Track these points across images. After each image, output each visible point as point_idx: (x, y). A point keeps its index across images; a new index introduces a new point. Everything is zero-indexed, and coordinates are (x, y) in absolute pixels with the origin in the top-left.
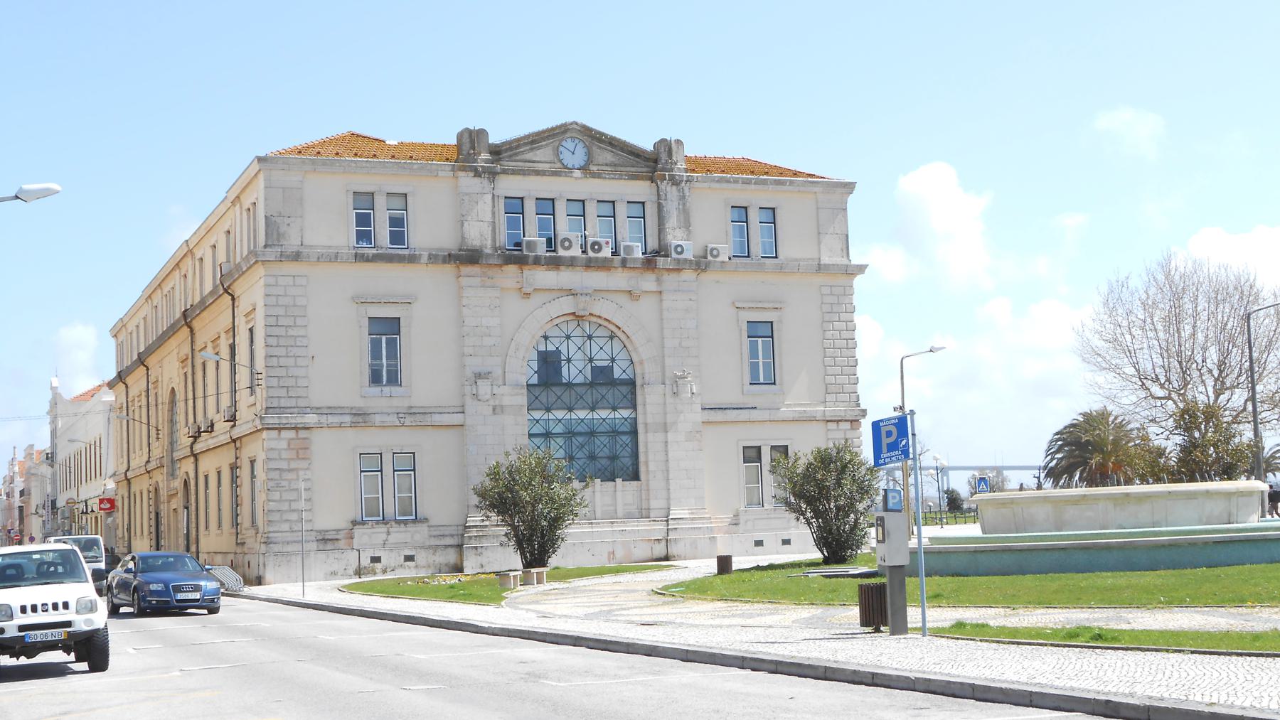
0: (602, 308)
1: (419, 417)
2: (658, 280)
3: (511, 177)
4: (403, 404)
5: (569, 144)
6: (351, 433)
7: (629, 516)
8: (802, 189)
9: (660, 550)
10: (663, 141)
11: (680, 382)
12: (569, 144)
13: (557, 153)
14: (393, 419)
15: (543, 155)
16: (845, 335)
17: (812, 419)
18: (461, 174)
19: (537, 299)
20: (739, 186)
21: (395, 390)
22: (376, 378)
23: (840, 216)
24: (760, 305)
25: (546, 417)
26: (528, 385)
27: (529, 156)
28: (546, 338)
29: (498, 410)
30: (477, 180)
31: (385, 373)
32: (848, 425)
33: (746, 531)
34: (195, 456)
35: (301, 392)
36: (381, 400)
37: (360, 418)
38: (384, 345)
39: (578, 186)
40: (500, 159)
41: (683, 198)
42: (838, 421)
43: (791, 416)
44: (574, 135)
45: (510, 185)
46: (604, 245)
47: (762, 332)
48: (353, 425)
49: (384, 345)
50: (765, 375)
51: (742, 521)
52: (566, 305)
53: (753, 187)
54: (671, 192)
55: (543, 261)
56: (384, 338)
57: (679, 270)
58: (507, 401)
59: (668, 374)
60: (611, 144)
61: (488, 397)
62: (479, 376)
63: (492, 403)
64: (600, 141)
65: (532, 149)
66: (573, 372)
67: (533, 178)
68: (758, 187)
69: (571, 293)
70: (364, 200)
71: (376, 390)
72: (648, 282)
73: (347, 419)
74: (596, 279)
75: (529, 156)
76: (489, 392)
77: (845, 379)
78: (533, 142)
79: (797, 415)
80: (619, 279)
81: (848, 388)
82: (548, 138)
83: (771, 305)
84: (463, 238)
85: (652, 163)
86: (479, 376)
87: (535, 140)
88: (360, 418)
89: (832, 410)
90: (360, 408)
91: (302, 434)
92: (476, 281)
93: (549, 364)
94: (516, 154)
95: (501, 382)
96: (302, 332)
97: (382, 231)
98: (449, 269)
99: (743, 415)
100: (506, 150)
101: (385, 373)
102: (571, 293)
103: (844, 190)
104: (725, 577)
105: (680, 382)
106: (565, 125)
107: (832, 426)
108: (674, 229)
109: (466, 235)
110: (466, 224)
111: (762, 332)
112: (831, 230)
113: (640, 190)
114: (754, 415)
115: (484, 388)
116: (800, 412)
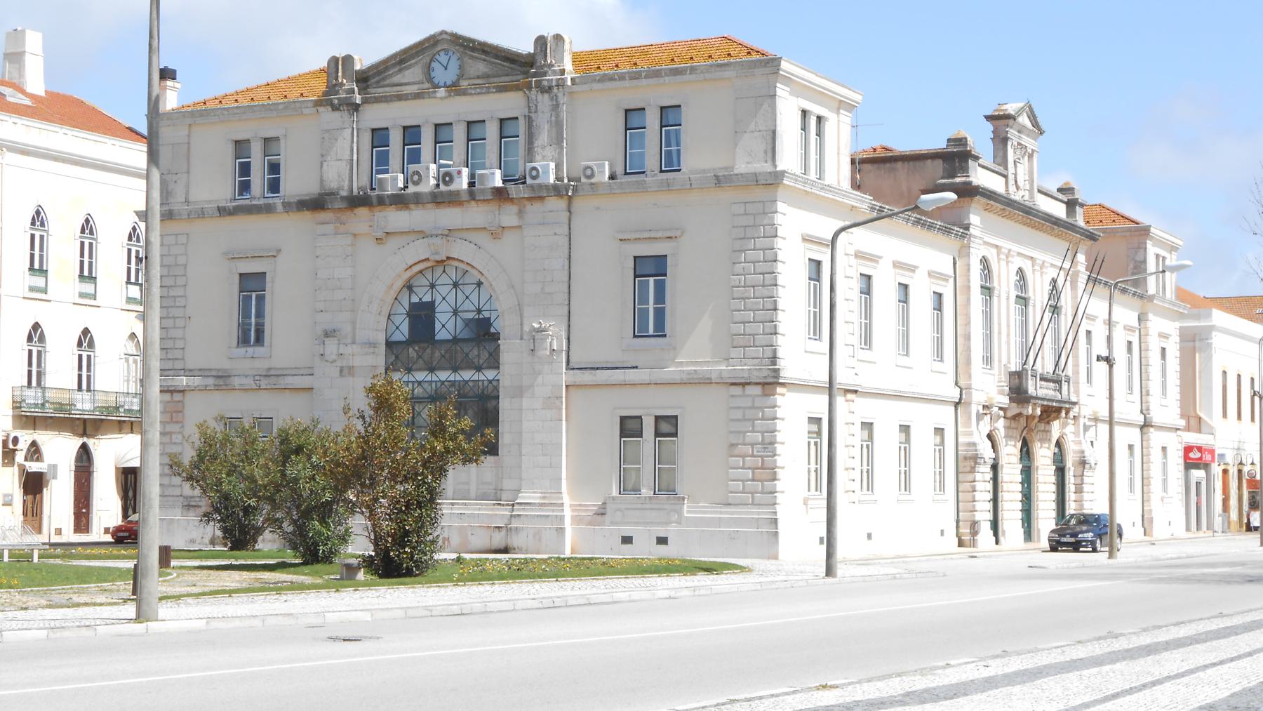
0: (460, 250)
1: (273, 379)
2: (521, 213)
3: (376, 106)
4: (262, 365)
5: (443, 58)
6: (217, 395)
7: (483, 497)
8: (708, 76)
9: (498, 540)
10: (334, 61)
11: (538, 336)
12: (443, 58)
13: (428, 70)
14: (249, 382)
15: (413, 74)
16: (761, 267)
17: (706, 382)
18: (321, 109)
19: (393, 243)
20: (627, 83)
21: (259, 350)
22: (244, 340)
23: (766, 106)
24: (646, 235)
25: (428, 378)
26: (390, 345)
27: (396, 79)
28: (479, 284)
29: (346, 371)
30: (337, 114)
31: (252, 333)
32: (757, 390)
33: (613, 523)
34: (831, 389)
35: (178, 354)
36: (247, 361)
37: (222, 381)
38: (254, 303)
39: (457, 109)
40: (368, 87)
41: (556, 107)
42: (744, 385)
43: (677, 378)
44: (445, 46)
45: (376, 115)
46: (455, 175)
47: (651, 269)
48: (218, 388)
49: (254, 303)
50: (651, 323)
51: (609, 511)
52: (419, 250)
53: (644, 82)
54: (544, 101)
55: (387, 201)
56: (254, 295)
57: (541, 198)
58: (357, 362)
59: (526, 328)
60: (484, 52)
61: (334, 357)
62: (328, 334)
63: (339, 363)
64: (473, 49)
65: (400, 70)
66: (445, 326)
67: (397, 104)
68: (650, 81)
69: (422, 234)
70: (241, 147)
71: (242, 351)
72: (508, 216)
73: (211, 381)
74: (449, 217)
75: (396, 79)
76: (335, 352)
77: (760, 328)
78: (401, 62)
79: (685, 377)
80: (475, 215)
81: (761, 339)
82: (417, 54)
83: (633, 236)
84: (322, 181)
85: (521, 69)
86: (328, 334)
87: (402, 59)
88: (222, 381)
89: (744, 369)
90: (225, 370)
91: (177, 397)
92: (329, 228)
93: (422, 316)
94: (384, 79)
95: (349, 341)
96: (180, 292)
97: (258, 179)
98: (307, 215)
99: (618, 376)
100: (374, 75)
101: (252, 333)
102: (422, 234)
103: (767, 70)
104: (830, 580)
105: (538, 336)
106: (432, 37)
107: (737, 390)
108: (544, 147)
109: (325, 178)
110: (325, 164)
111: (651, 269)
112: (752, 127)
113: (511, 103)
114: (631, 375)
115: (331, 347)
116: (689, 373)
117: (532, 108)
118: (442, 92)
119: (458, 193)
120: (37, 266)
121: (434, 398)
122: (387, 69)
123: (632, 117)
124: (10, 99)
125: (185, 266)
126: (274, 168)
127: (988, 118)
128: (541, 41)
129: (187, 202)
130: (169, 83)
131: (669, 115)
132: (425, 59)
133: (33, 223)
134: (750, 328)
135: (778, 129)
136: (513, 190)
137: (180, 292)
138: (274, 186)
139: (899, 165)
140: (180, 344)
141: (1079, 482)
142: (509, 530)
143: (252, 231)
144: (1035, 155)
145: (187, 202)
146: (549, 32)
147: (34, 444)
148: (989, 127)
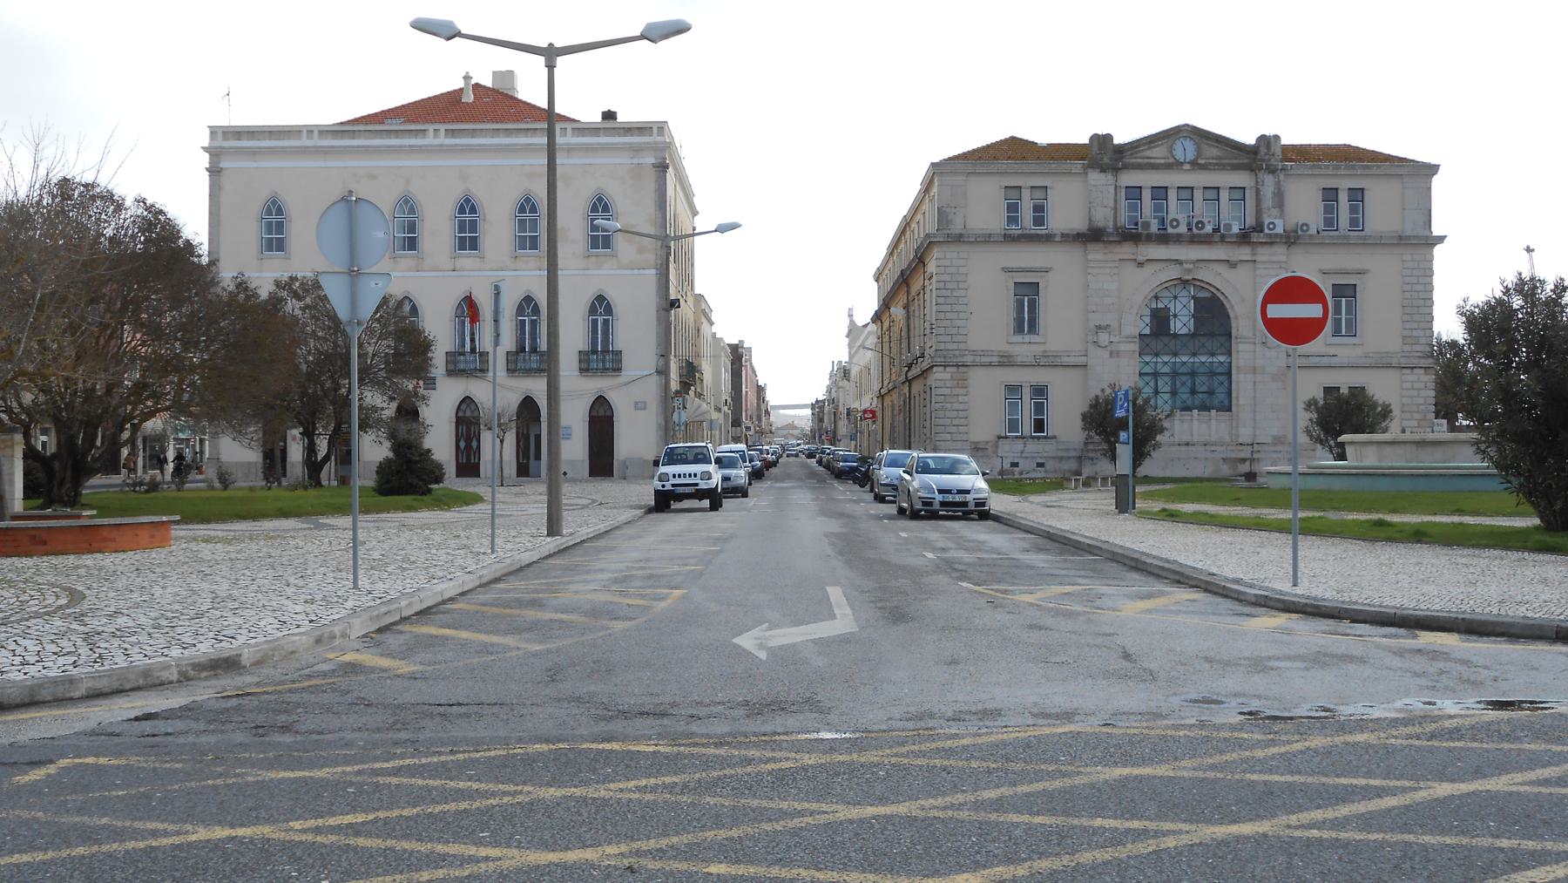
21: (1034, 338)
22: (1019, 329)
27: (1148, 153)
28: (1156, 297)
35: (961, 338)
36: (1024, 348)
39: (1198, 179)
45: (1130, 179)
69: (1178, 262)
71: (1018, 338)
77: (1421, 333)
97: (1027, 214)
115: (1104, 338)
121: (1193, 374)
123: (1330, 195)
131: (1357, 195)
134: (1415, 333)
137: (962, 293)
138: (1039, 221)
142: (1252, 460)
143: (1028, 257)
147: (601, 402)
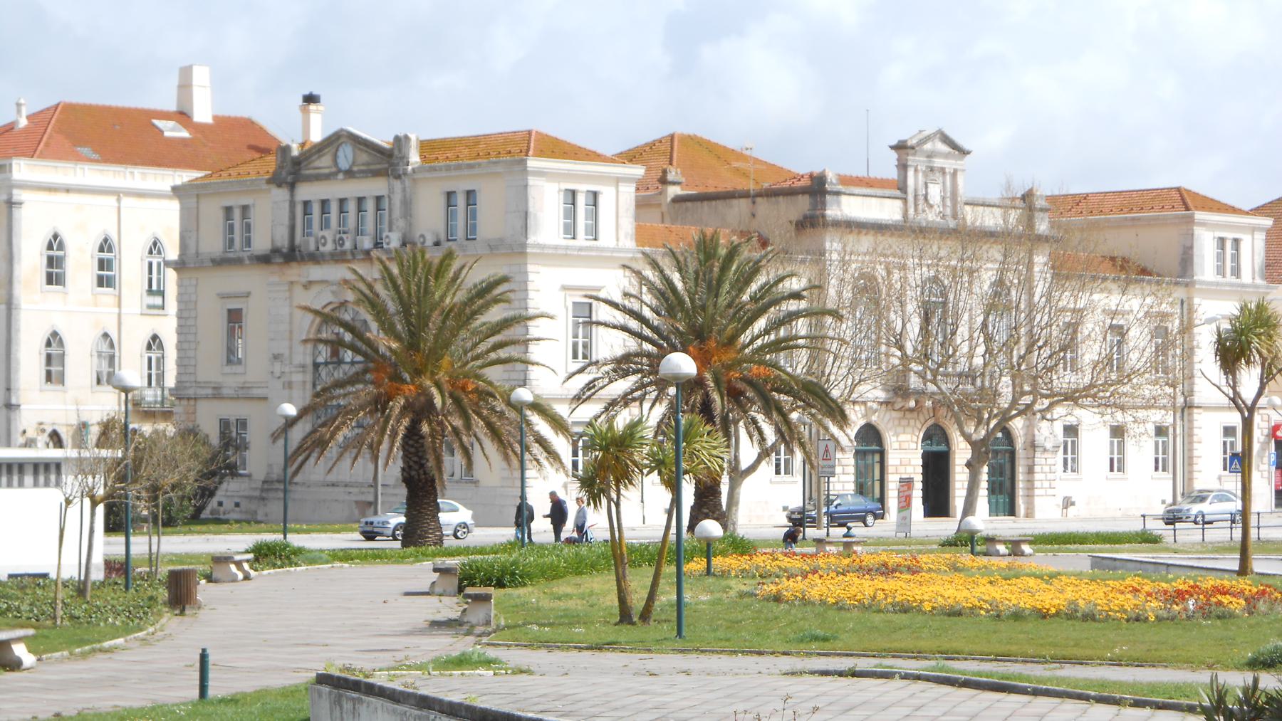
19: (315, 289)
35: (191, 370)
71: (228, 369)
85: (386, 160)
91: (192, 402)
117: (391, 191)
118: (341, 176)
119: (344, 253)
120: (154, 287)
122: (311, 156)
124: (167, 134)
125: (196, 302)
126: (248, 228)
127: (894, 148)
128: (397, 139)
129: (197, 254)
130: (312, 107)
132: (331, 150)
133: (151, 252)
135: (531, 209)
136: (375, 253)
139: (781, 198)
140: (193, 362)
141: (1030, 462)
144: (959, 174)
145: (197, 254)
146: (401, 134)
148: (894, 155)
